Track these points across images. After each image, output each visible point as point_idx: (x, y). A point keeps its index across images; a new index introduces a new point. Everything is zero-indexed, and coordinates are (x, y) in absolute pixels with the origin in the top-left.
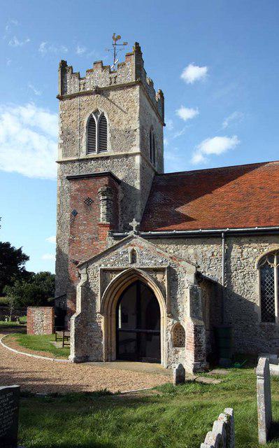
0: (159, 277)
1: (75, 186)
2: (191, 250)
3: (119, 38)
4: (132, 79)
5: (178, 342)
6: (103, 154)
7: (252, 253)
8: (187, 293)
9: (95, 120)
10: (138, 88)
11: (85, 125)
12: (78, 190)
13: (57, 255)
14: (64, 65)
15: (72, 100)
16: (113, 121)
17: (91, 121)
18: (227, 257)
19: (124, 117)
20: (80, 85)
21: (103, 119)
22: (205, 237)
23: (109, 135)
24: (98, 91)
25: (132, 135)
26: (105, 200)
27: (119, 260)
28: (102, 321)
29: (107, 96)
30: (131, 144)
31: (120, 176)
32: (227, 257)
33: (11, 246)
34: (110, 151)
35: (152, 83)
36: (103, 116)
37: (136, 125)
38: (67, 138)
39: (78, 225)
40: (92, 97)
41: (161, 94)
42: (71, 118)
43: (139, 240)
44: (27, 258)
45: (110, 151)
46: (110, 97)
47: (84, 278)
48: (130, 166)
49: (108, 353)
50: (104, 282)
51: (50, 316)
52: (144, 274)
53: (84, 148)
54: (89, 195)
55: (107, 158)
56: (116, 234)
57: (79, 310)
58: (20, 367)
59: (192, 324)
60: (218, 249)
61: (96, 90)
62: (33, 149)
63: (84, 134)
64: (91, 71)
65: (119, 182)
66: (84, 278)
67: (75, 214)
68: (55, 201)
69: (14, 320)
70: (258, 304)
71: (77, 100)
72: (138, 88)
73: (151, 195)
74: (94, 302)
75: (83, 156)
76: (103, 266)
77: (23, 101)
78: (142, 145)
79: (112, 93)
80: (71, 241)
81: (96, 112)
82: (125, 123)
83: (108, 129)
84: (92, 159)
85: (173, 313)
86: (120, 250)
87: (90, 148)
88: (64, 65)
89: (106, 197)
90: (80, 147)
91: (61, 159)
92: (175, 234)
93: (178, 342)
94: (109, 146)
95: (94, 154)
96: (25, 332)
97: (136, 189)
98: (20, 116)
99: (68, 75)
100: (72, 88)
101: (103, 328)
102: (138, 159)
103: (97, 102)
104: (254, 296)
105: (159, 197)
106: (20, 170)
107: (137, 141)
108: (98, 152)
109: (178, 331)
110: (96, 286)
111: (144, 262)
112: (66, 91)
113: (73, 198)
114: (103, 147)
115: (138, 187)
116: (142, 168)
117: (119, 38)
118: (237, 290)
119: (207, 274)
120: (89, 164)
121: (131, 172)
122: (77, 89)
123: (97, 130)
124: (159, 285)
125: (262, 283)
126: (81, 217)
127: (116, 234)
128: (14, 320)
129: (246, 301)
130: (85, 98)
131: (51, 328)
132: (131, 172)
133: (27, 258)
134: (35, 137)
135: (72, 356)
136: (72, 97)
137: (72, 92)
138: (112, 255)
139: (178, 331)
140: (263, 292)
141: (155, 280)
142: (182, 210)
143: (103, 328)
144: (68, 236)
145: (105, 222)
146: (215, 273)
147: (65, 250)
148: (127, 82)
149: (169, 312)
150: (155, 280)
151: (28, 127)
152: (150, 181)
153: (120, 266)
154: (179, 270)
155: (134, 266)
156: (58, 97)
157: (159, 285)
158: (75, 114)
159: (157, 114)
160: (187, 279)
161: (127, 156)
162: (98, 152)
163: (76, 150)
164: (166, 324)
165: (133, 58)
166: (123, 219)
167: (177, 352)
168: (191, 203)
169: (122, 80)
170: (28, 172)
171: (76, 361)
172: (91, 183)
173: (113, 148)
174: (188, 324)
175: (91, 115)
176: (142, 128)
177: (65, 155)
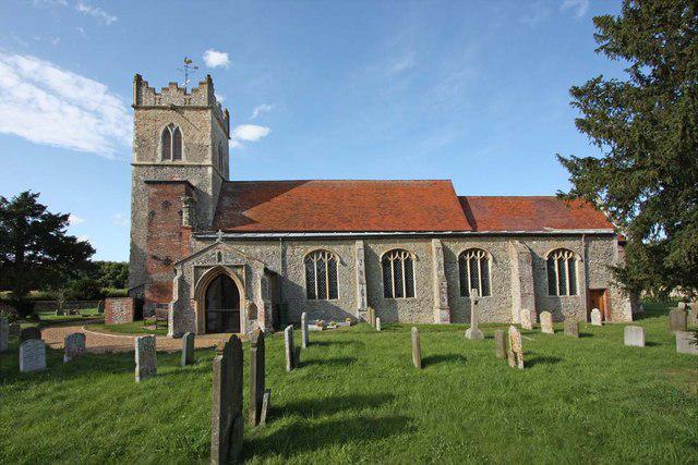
0: (239, 271)
1: (153, 190)
2: (257, 250)
3: (190, 62)
4: (204, 103)
5: (253, 315)
6: (177, 162)
7: (301, 252)
8: (259, 281)
10: (210, 111)
11: (160, 135)
14: (139, 79)
17: (166, 132)
18: (284, 255)
23: (183, 147)
24: (174, 108)
27: (210, 260)
28: (195, 306)
30: (204, 157)
31: (194, 183)
32: (284, 255)
33: (79, 240)
34: (184, 160)
35: (220, 105)
36: (177, 130)
37: (208, 141)
38: (142, 143)
41: (227, 112)
43: (224, 245)
44: (94, 252)
45: (184, 160)
47: (179, 273)
48: (203, 175)
49: (200, 329)
50: (197, 276)
51: (131, 306)
52: (228, 269)
53: (160, 155)
55: (183, 166)
57: (176, 297)
58: (119, 343)
59: (262, 303)
60: (277, 248)
62: (40, 109)
64: (167, 89)
65: (193, 187)
66: (179, 273)
67: (152, 214)
68: (128, 201)
69: (60, 313)
70: (305, 287)
71: (152, 112)
72: (210, 111)
73: (221, 198)
74: (188, 291)
75: (158, 162)
76: (196, 264)
77: (25, 52)
78: (213, 159)
79: (186, 112)
80: (149, 238)
81: (172, 125)
85: (249, 296)
86: (210, 252)
87: (165, 156)
88: (139, 79)
90: (155, 154)
91: (136, 162)
93: (253, 315)
94: (183, 156)
95: (167, 162)
96: (103, 322)
98: (16, 67)
99: (144, 89)
100: (147, 100)
101: (196, 311)
102: (210, 170)
103: (172, 116)
104: (302, 282)
105: (227, 201)
106: (21, 132)
107: (210, 155)
109: (253, 308)
110: (190, 278)
111: (227, 261)
113: (151, 200)
114: (177, 156)
115: (210, 193)
116: (214, 177)
117: (190, 62)
118: (290, 278)
119: (270, 267)
121: (205, 181)
123: (172, 142)
124: (240, 278)
125: (307, 273)
128: (60, 313)
129: (297, 286)
131: (131, 316)
132: (205, 181)
133: (94, 252)
134: (41, 95)
135: (171, 333)
136: (147, 108)
138: (203, 257)
139: (253, 308)
140: (308, 279)
141: (236, 274)
142: (246, 213)
143: (196, 311)
144: (144, 231)
146: (276, 267)
147: (142, 245)
148: (201, 105)
149: (246, 295)
150: (236, 274)
151: (30, 81)
152: (220, 186)
153: (210, 264)
154: (253, 267)
155: (221, 264)
156: (133, 106)
157: (240, 278)
159: (224, 130)
160: (259, 273)
161: (200, 166)
163: (151, 155)
164: (244, 305)
165: (206, 86)
166: (535, 404)
167: (252, 323)
168: (254, 208)
169: (194, 103)
170: (34, 135)
171: (174, 337)
172: (169, 188)
174: (260, 303)
176: (213, 145)
177: (140, 159)
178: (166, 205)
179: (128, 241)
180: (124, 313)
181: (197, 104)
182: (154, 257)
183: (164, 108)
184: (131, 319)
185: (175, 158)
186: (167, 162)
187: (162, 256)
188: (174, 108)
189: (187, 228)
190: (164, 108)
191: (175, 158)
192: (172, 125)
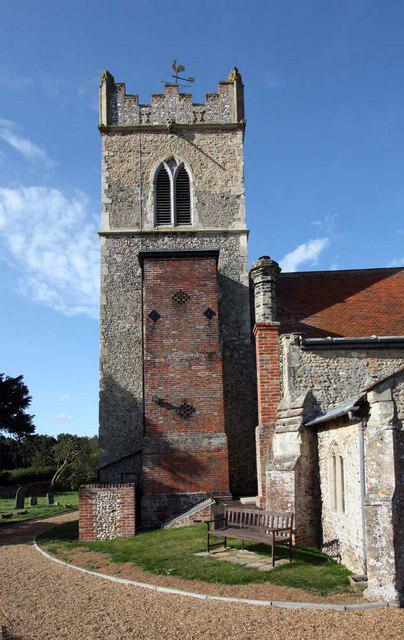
3: (182, 69)
6: (182, 228)
9: (170, 173)
11: (151, 178)
12: (158, 277)
13: (102, 394)
14: (110, 79)
15: (128, 137)
16: (201, 178)
17: (162, 177)
19: (219, 174)
20: (141, 114)
21: (182, 176)
22: (381, 348)
23: (193, 200)
24: (175, 129)
25: (235, 203)
26: (268, 282)
29: (190, 139)
34: (195, 224)
39: (162, 336)
40: (163, 136)
42: (125, 166)
45: (195, 224)
46: (195, 142)
53: (151, 216)
54: (180, 287)
56: (311, 340)
61: (171, 127)
63: (150, 194)
71: (134, 139)
72: (240, 134)
75: (148, 227)
79: (198, 136)
81: (171, 161)
82: (220, 183)
83: (192, 189)
84: (166, 234)
87: (161, 217)
88: (110, 79)
89: (269, 278)
90: (143, 213)
91: (107, 229)
92: (375, 342)
95: (164, 228)
97: (242, 286)
99: (120, 95)
100: (126, 118)
103: (171, 146)
108: (176, 225)
112: (116, 121)
114: (183, 216)
117: (182, 69)
120: (160, 241)
122: (137, 120)
126: (166, 322)
127: (311, 340)
130: (150, 137)
136: (126, 131)
137: (127, 124)
145: (268, 321)
147: (133, 385)
158: (132, 161)
161: (226, 234)
162: (176, 225)
163: (135, 217)
169: (212, 118)
172: (185, 267)
173: (201, 220)
175: (162, 165)
178: (181, 299)
179: (96, 377)
180: (118, 515)
181: (216, 120)
182: (161, 403)
183: (156, 130)
184: (132, 529)
185: (178, 221)
186: (164, 228)
187: (175, 397)
188: (175, 129)
189: (267, 327)
190: (156, 130)
191: (178, 221)
192: (171, 161)
